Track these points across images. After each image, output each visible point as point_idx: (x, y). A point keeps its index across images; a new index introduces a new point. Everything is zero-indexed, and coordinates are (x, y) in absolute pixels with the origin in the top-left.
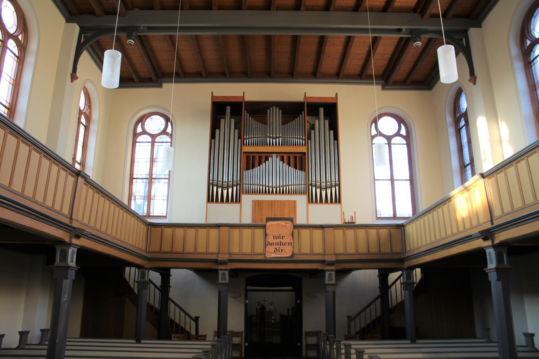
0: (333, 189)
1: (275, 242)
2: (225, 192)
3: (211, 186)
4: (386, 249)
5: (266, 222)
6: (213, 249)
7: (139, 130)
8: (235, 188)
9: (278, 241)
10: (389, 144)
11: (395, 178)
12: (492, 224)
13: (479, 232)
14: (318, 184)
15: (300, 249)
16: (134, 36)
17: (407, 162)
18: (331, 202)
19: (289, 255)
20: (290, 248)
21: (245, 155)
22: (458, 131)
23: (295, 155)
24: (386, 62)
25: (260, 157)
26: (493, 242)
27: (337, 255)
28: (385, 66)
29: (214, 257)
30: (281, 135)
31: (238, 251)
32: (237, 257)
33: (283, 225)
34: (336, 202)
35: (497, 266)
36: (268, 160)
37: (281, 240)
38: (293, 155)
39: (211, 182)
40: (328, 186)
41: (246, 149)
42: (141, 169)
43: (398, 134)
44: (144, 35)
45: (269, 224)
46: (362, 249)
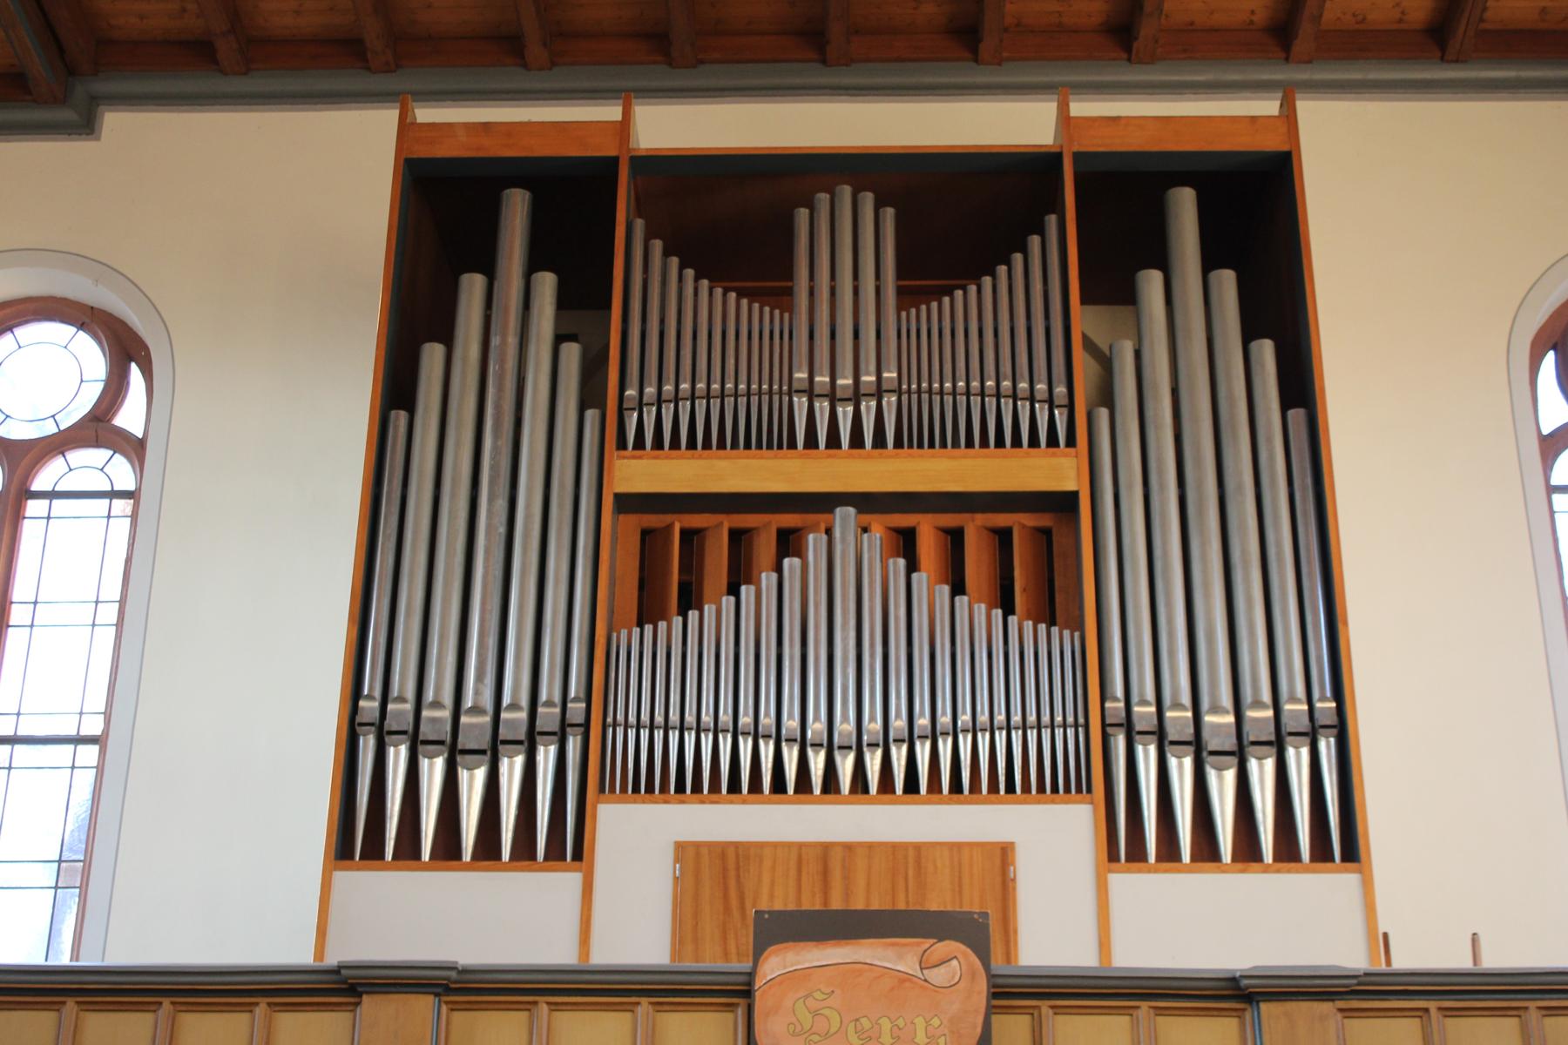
0: (1299, 759)
2: (472, 783)
3: (367, 745)
8: (546, 757)
14: (1179, 718)
21: (634, 523)
23: (1001, 520)
25: (739, 538)
30: (890, 375)
33: (904, 979)
34: (1322, 852)
36: (800, 552)
39: (369, 706)
40: (1251, 734)
45: (777, 963)
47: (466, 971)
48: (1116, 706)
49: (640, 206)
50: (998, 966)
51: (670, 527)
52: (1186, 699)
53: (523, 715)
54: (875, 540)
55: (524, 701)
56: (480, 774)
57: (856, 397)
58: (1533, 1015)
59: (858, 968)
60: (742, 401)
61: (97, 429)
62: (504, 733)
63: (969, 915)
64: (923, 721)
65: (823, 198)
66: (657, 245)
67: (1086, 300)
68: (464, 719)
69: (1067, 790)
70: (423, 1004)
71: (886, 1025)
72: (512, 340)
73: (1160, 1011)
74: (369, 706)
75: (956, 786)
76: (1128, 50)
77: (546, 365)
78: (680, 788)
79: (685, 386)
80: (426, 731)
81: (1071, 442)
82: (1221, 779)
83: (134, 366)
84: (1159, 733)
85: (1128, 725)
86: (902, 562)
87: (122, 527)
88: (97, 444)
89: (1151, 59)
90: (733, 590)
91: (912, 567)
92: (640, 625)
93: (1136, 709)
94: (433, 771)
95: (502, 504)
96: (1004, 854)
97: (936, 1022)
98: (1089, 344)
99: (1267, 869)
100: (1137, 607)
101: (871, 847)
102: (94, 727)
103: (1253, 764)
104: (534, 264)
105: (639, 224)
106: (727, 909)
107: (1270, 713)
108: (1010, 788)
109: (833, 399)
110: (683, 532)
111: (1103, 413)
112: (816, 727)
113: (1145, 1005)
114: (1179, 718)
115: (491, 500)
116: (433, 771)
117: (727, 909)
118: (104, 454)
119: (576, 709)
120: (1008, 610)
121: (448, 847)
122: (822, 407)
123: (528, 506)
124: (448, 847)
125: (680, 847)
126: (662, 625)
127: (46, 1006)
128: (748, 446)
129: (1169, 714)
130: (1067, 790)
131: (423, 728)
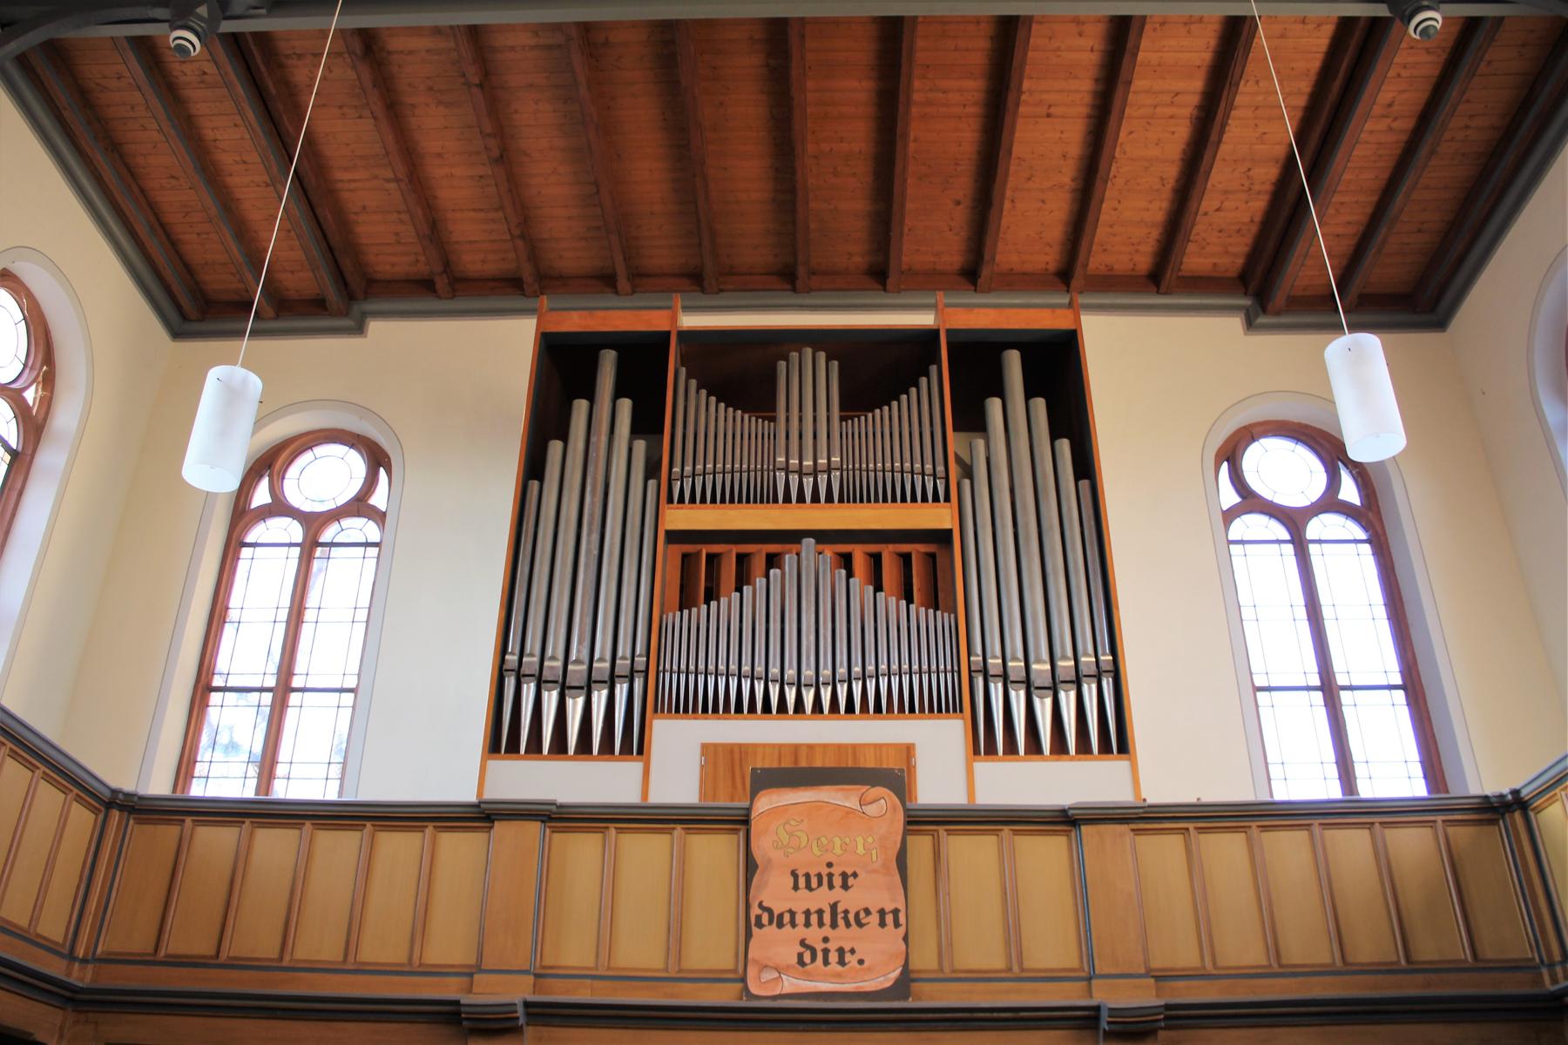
0: (1090, 691)
1: (799, 909)
2: (575, 707)
3: (510, 683)
4: (1440, 942)
5: (754, 795)
6: (449, 945)
7: (261, 495)
8: (621, 691)
9: (821, 898)
10: (1300, 545)
11: (1341, 680)
14: (1016, 665)
15: (945, 947)
16: (200, 18)
17: (1381, 612)
18: (1084, 747)
19: (884, 979)
20: (891, 939)
21: (678, 550)
23: (905, 548)
24: (1259, 204)
25: (742, 559)
27: (1162, 977)
28: (1254, 229)
29: (448, 990)
30: (836, 459)
31: (589, 961)
32: (584, 994)
33: (849, 812)
34: (1105, 748)
36: (780, 566)
37: (838, 893)
38: (892, 547)
39: (512, 659)
40: (1061, 675)
41: (681, 518)
42: (247, 653)
43: (1329, 503)
44: (256, 35)
45: (767, 802)
46: (1306, 943)
47: (562, 806)
49: (684, 360)
50: (909, 805)
51: (699, 553)
52: (1020, 654)
53: (607, 665)
55: (608, 656)
56: (581, 701)
57: (815, 473)
58: (1255, 831)
60: (745, 475)
62: (595, 676)
63: (893, 775)
64: (857, 669)
65: (794, 355)
66: (693, 383)
68: (570, 667)
69: (947, 710)
70: (534, 827)
71: (838, 841)
72: (604, 439)
73: (1016, 833)
75: (878, 709)
76: (975, 285)
77: (624, 451)
78: (705, 710)
79: (710, 466)
80: (547, 675)
81: (947, 499)
82: (1043, 704)
83: (382, 470)
85: (985, 671)
86: (843, 572)
87: (371, 564)
88: (359, 515)
89: (989, 290)
90: (739, 589)
91: (850, 575)
92: (681, 610)
93: (990, 661)
94: (551, 699)
95: (596, 537)
96: (908, 750)
97: (870, 840)
99: (1072, 759)
100: (989, 598)
101: (825, 746)
103: (1062, 695)
104: (619, 393)
105: (683, 370)
106: (734, 786)
107: (1072, 663)
108: (912, 710)
109: (801, 474)
110: (708, 555)
111: (967, 482)
112: (791, 673)
113: (1006, 828)
115: (589, 534)
116: (551, 699)
117: (734, 786)
118: (362, 521)
119: (640, 661)
120: (910, 601)
122: (794, 478)
123: (612, 538)
126: (694, 610)
127: (292, 826)
128: (748, 501)
129: (1010, 664)
130: (947, 710)
131: (545, 673)
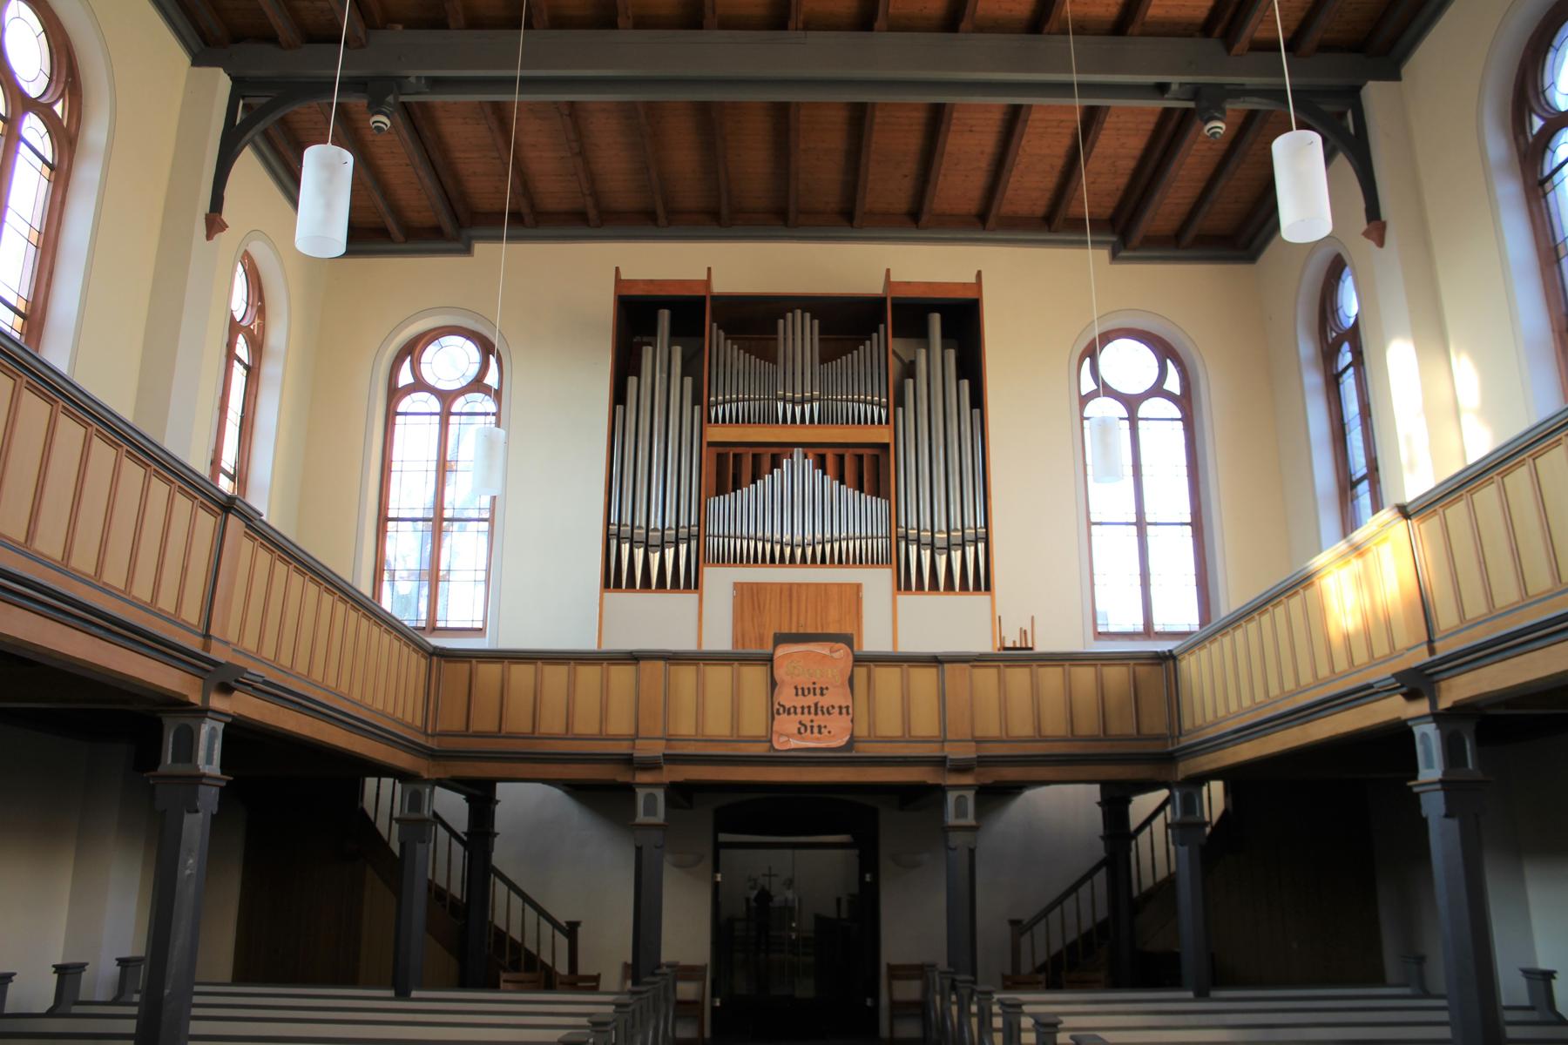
0: (970, 550)
1: (799, 705)
2: (655, 558)
3: (614, 543)
4: (1122, 725)
5: (775, 646)
6: (620, 724)
7: (405, 377)
8: (683, 548)
9: (810, 700)
10: (1133, 420)
11: (1149, 519)
12: (1432, 651)
13: (1394, 675)
14: (926, 535)
15: (872, 725)
16: (389, 104)
17: (1183, 471)
18: (964, 587)
19: (841, 741)
20: (845, 721)
21: (714, 450)
22: (1333, 382)
23: (859, 451)
24: (1122, 181)
25: (756, 457)
26: (1433, 704)
27: (979, 741)
28: (1119, 194)
29: (623, 748)
30: (816, 393)
31: (693, 732)
32: (691, 749)
33: (825, 656)
34: (977, 587)
35: (1445, 773)
36: (780, 466)
37: (818, 698)
38: (851, 451)
39: (614, 528)
40: (953, 541)
41: (716, 434)
42: (411, 492)
43: (1157, 390)
44: (418, 103)
45: (782, 651)
46: (1054, 725)
48: (902, 531)
49: (713, 320)
54: (809, 463)
59: (808, 653)
61: (477, 385)
67: (894, 336)
70: (661, 663)
74: (614, 528)
75: (840, 561)
84: (918, 541)
89: (926, 228)
98: (894, 352)
101: (808, 585)
102: (486, 515)
112: (787, 538)
114: (926, 535)
116: (639, 553)
121: (646, 583)
124: (646, 583)
125: (736, 585)
